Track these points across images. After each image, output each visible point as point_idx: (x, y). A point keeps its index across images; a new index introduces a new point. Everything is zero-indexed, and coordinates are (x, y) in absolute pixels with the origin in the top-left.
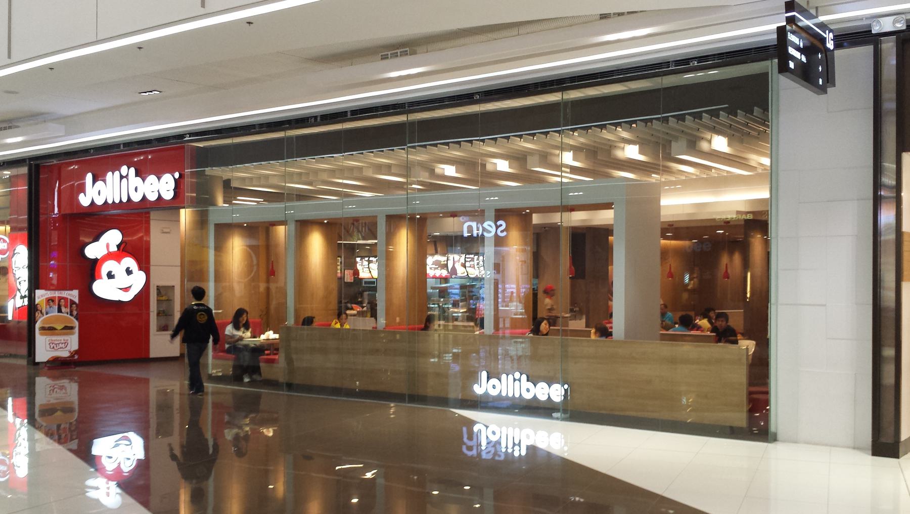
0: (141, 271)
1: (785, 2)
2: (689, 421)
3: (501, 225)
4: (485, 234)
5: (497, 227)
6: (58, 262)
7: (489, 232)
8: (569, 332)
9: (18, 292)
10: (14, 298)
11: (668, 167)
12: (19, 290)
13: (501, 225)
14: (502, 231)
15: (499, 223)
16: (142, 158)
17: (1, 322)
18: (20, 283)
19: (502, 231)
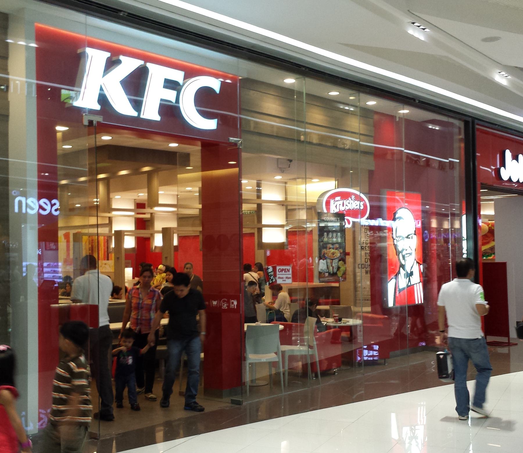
0: (153, 390)
1: (164, 87)
2: (407, 204)
3: (55, 204)
4: (29, 211)
5: (52, 205)
6: (57, 183)
7: (32, 209)
8: (40, 277)
9: (401, 269)
10: (397, 276)
11: (380, 237)
12: (403, 266)
13: (55, 204)
14: (56, 210)
15: (54, 201)
16: (437, 128)
17: (467, 450)
18: (404, 257)
19: (56, 210)
